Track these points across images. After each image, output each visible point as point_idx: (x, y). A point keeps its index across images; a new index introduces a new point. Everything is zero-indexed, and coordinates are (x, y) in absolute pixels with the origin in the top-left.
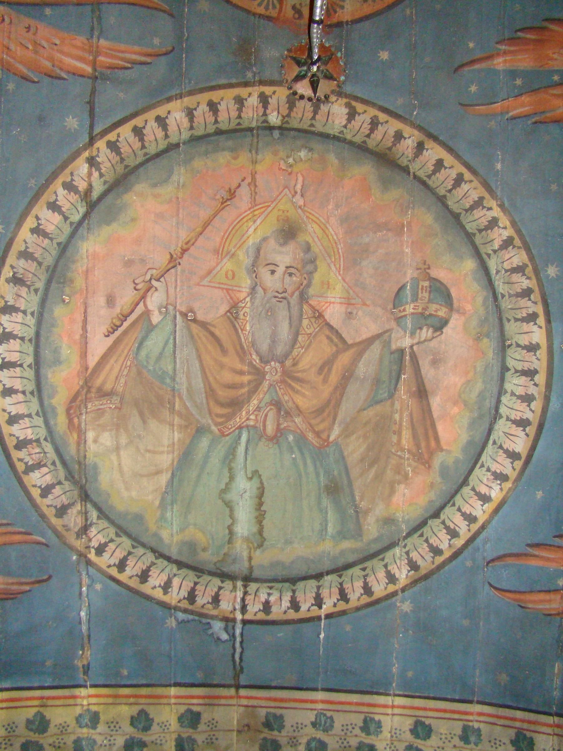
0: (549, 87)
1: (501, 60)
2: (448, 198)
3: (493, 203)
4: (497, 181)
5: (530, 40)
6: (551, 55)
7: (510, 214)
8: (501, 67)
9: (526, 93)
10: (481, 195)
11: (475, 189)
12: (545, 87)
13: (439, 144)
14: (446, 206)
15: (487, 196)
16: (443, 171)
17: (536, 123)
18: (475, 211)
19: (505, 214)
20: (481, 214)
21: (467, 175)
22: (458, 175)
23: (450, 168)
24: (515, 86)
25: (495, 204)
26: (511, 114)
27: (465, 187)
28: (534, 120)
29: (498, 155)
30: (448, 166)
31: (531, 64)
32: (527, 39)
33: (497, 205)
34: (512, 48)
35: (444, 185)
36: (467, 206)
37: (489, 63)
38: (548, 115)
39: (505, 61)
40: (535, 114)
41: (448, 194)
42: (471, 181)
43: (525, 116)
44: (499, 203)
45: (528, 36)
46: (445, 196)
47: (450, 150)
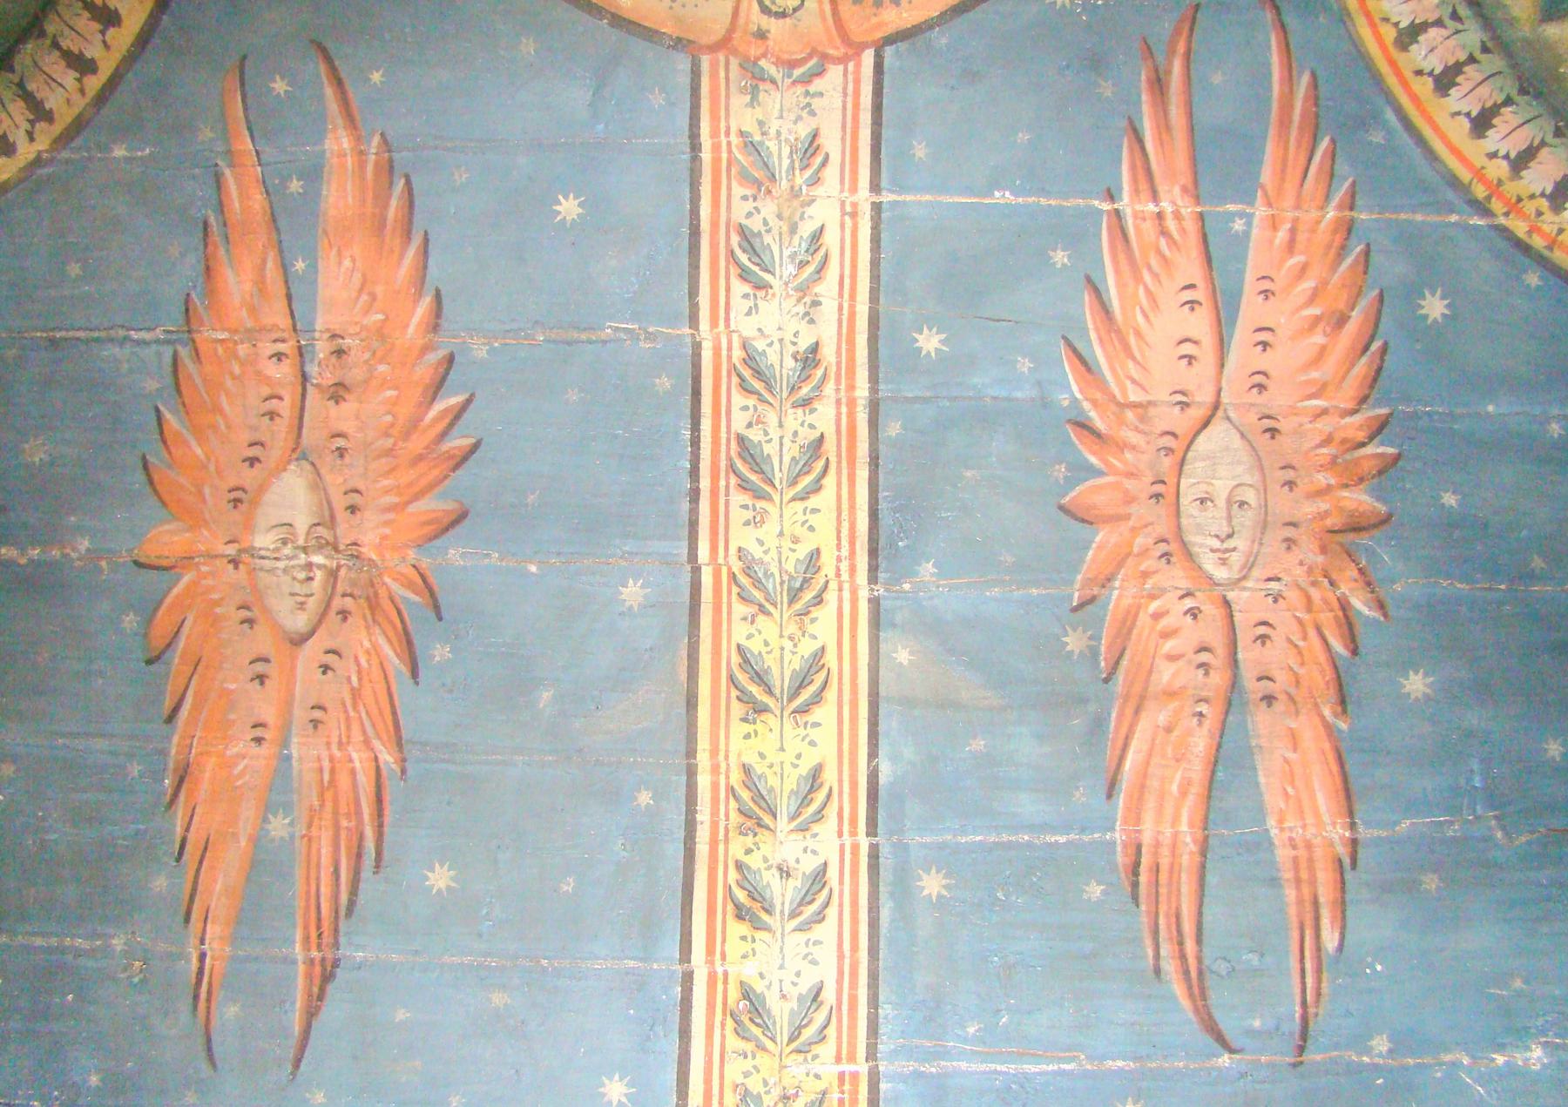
0: (281, 251)
1: (346, 143)
2: (39, 42)
3: (42, 144)
4: (88, 150)
5: (386, 206)
6: (347, 253)
7: (21, 181)
8: (329, 145)
9: (271, 203)
10: (56, 116)
11: (68, 100)
12: (206, 246)
13: (151, 15)
14: (22, 38)
15: (58, 128)
16: (97, 26)
17: (206, 224)
18: (22, 104)
19: (21, 170)
20: (19, 119)
21: (94, 83)
22: (93, 61)
23: (104, 42)
24: (285, 180)
25: (40, 148)
26: (227, 172)
27: (69, 78)
28: (212, 220)
29: (143, 150)
30: (108, 38)
31: (332, 212)
32: (390, 196)
33: (40, 152)
34: (370, 168)
35: (67, 31)
36: (31, 87)
37: (340, 122)
38: (222, 252)
39: (342, 155)
40: (225, 225)
41: (48, 42)
42: (82, 91)
43: (221, 203)
44: (45, 155)
45: (394, 202)
46: (42, 34)
47: (143, 40)
